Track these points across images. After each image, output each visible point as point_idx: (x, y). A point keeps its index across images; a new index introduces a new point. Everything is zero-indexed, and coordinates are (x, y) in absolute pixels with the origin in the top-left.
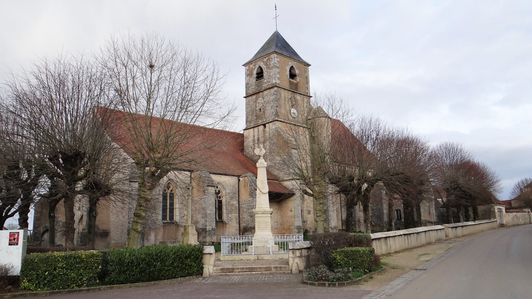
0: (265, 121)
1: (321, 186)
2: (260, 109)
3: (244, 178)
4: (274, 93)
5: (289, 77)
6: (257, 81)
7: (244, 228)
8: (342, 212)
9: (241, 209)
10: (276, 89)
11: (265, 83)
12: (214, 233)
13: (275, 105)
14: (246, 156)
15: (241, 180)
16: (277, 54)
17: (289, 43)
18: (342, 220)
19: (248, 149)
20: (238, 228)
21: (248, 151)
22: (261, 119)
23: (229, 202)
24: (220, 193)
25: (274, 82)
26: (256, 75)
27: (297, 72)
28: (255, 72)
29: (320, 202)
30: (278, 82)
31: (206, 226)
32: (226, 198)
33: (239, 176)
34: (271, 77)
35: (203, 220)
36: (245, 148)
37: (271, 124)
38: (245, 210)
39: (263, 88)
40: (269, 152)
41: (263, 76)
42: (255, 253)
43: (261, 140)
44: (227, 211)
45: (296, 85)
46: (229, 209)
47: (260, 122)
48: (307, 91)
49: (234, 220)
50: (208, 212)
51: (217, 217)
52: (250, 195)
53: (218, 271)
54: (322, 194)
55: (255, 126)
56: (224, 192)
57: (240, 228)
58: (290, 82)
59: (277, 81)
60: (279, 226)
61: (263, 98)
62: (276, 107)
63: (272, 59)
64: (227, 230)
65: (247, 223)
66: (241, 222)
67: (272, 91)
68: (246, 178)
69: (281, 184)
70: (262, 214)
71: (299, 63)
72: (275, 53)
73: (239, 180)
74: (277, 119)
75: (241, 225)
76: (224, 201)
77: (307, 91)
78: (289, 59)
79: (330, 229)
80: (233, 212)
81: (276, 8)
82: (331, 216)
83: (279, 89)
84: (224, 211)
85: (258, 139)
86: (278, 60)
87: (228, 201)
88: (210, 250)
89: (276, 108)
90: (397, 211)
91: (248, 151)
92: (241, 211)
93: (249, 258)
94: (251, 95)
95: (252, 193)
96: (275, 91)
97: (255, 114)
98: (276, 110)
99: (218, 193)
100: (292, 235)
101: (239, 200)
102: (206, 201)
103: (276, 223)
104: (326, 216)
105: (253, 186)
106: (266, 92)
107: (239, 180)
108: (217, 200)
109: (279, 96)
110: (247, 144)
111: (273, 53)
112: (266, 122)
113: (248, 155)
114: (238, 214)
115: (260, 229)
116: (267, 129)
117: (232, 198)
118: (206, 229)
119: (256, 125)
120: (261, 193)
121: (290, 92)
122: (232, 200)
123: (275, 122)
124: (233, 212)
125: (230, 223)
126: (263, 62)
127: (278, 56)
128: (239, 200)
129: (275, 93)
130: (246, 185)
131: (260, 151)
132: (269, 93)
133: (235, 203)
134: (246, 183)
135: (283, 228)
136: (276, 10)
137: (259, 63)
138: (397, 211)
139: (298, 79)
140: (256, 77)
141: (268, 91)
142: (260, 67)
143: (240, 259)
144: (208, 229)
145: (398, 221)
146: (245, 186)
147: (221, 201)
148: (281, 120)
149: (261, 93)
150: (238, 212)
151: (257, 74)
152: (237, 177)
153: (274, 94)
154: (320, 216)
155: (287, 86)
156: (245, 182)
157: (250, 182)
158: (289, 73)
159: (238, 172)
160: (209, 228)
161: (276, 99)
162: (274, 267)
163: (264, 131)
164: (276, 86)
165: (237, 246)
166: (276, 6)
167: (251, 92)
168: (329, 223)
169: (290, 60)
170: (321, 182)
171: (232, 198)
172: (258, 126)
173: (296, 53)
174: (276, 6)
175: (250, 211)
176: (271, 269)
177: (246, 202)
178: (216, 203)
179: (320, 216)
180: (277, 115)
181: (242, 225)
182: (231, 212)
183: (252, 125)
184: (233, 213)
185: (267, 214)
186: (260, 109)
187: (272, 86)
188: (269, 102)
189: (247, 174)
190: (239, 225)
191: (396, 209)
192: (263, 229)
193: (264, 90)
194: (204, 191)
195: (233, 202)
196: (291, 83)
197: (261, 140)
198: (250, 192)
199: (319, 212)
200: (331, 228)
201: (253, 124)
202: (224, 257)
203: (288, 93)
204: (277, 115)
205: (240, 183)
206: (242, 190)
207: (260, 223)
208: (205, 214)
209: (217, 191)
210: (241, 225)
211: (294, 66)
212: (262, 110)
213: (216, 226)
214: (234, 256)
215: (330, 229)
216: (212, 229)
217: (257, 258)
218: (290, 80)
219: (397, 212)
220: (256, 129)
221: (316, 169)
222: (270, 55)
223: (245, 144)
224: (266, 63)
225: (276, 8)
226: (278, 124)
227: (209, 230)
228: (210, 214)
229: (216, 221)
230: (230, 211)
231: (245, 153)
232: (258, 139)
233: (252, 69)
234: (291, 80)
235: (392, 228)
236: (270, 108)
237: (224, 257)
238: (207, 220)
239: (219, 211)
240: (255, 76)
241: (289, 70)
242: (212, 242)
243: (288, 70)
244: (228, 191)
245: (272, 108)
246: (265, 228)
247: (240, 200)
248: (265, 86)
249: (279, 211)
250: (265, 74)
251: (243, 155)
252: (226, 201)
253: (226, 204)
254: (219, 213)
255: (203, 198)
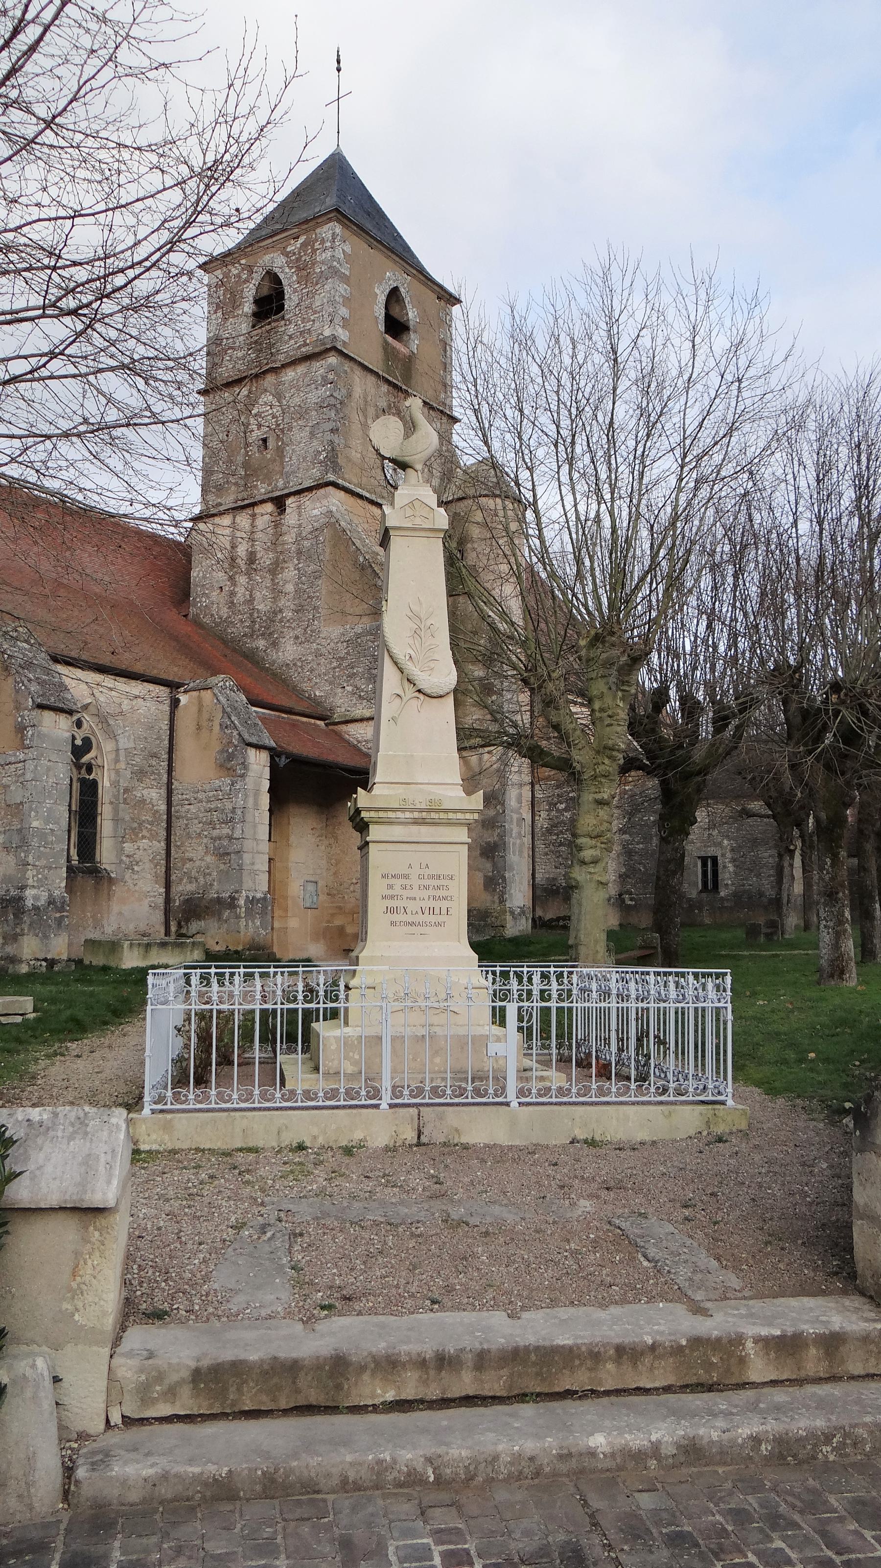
0: (280, 486)
1: (608, 721)
2: (265, 441)
3: (195, 694)
4: (324, 378)
5: (382, 327)
6: (253, 326)
7: (187, 901)
8: (537, 855)
9: (178, 826)
10: (333, 360)
11: (291, 337)
12: (59, 921)
13: (330, 426)
14: (197, 623)
15: (181, 704)
16: (345, 226)
17: (381, 206)
18: (534, 886)
19: (207, 596)
20: (161, 901)
21: (205, 601)
22: (268, 478)
23: (126, 791)
24: (89, 751)
25: (327, 333)
26: (253, 307)
27: (412, 315)
28: (249, 292)
29: (598, 796)
30: (343, 335)
31: (23, 888)
32: (117, 772)
33: (173, 686)
34: (315, 312)
35: (11, 859)
36: (195, 591)
37: (306, 499)
38: (196, 827)
39: (281, 357)
40: (292, 607)
41: (281, 308)
42: (394, 1095)
43: (266, 559)
44: (115, 829)
45: (408, 364)
46: (127, 818)
47: (262, 489)
48: (442, 396)
49: (148, 866)
50: (35, 824)
51: (74, 852)
52: (221, 766)
53: (171, 1393)
54: (609, 757)
55: (240, 503)
56: (108, 746)
57: (168, 900)
58: (386, 346)
59: (340, 330)
60: (323, 898)
61: (279, 396)
62: (332, 431)
63: (323, 241)
64: (115, 907)
65: (202, 880)
66: (173, 877)
67: (319, 368)
68: (207, 695)
69: (339, 736)
70: (416, 822)
71: (420, 281)
72: (339, 221)
73: (175, 703)
74: (331, 477)
75: (176, 889)
76: (107, 783)
77: (442, 396)
78: (388, 257)
79: (509, 917)
80: (145, 833)
81: (338, 62)
82: (512, 869)
83: (347, 366)
84: (106, 826)
85: (252, 558)
86: (348, 248)
87: (123, 784)
88: (88, 1162)
89: (329, 436)
90: (704, 860)
91: (205, 601)
92: (177, 832)
93: (358, 1135)
94: (229, 385)
95: (231, 757)
96: (331, 369)
97: (240, 459)
98: (331, 442)
99: (80, 749)
100: (696, 976)
101: (169, 784)
102: (29, 776)
103: (311, 887)
104: (495, 866)
105: (236, 728)
106: (290, 375)
107: (175, 703)
108: (75, 780)
109: (344, 391)
110: (204, 577)
111: (330, 220)
112: (286, 491)
113: (207, 620)
114: (163, 844)
115: (396, 917)
116: (291, 517)
117: (140, 774)
118: (21, 899)
119: (246, 502)
120: (410, 691)
121: (385, 388)
122: (140, 780)
123: (322, 491)
124: (145, 833)
125: (127, 877)
126: (287, 255)
127: (347, 233)
128: (169, 784)
129: (331, 376)
130: (204, 724)
131: (407, 436)
132: (306, 375)
133: (155, 795)
134: (205, 716)
135: (340, 908)
136: (339, 70)
137: (267, 258)
138: (704, 860)
139: (414, 341)
140: (255, 314)
141: (301, 369)
142: (273, 278)
143: (290, 1138)
144: (29, 903)
145: (704, 895)
146: (199, 728)
147: (94, 783)
148: (347, 485)
149: (270, 379)
150: (163, 833)
151: (257, 302)
152: (168, 690)
153: (325, 381)
154: (595, 862)
155: (374, 360)
156: (200, 711)
157: (224, 711)
158: (383, 311)
159: (172, 673)
160: (36, 898)
161: (332, 401)
162: (766, 1343)
163: (277, 525)
164: (334, 348)
165: (247, 1036)
166: (338, 56)
167: (227, 371)
168: (503, 893)
169: (389, 263)
170: (608, 701)
171: (140, 774)
172: (253, 505)
173: (407, 249)
174: (338, 56)
175: (216, 833)
176: (742, 1361)
177: (200, 796)
178: (71, 785)
179: (595, 862)
180: (332, 460)
181: (180, 888)
182: (136, 835)
183: (228, 501)
184: (144, 837)
185: (450, 823)
186: (265, 441)
187: (317, 350)
188: (302, 413)
189: (213, 680)
190: (168, 886)
191: (703, 854)
192: (420, 918)
193: (284, 366)
194: (21, 729)
195: (145, 792)
196: (389, 353)
197: (266, 559)
198: (222, 751)
199: (594, 842)
200: (512, 913)
201: (232, 498)
202: (167, 1127)
203: (378, 387)
204: (332, 460)
205: (179, 713)
206: (187, 746)
207: (398, 883)
208: (20, 831)
209: (79, 742)
210: (174, 889)
211: (402, 290)
212: (271, 444)
213: (69, 888)
214: (242, 1120)
215: (509, 917)
216: (51, 902)
217: (410, 1135)
218: (386, 342)
219: (704, 865)
220: (243, 520)
221: (583, 643)
222: (319, 225)
223: (194, 574)
224: (298, 260)
225: (338, 62)
226: (335, 500)
227: (36, 908)
228: (42, 835)
229: (70, 869)
230: (133, 829)
231: (192, 610)
232: (252, 558)
233: (240, 282)
234: (390, 339)
235: (873, 926)
236: (306, 433)
237: (167, 1127)
238: (30, 859)
239: (81, 825)
240: (248, 307)
241: (384, 298)
242: (45, 960)
243: (382, 299)
244: (124, 743)
245: (312, 435)
246: (432, 919)
247: (176, 785)
248: (288, 348)
249: (326, 842)
250: (291, 300)
251: (185, 616)
252: (115, 784)
253: (116, 797)
254: (80, 834)
255: (13, 759)
